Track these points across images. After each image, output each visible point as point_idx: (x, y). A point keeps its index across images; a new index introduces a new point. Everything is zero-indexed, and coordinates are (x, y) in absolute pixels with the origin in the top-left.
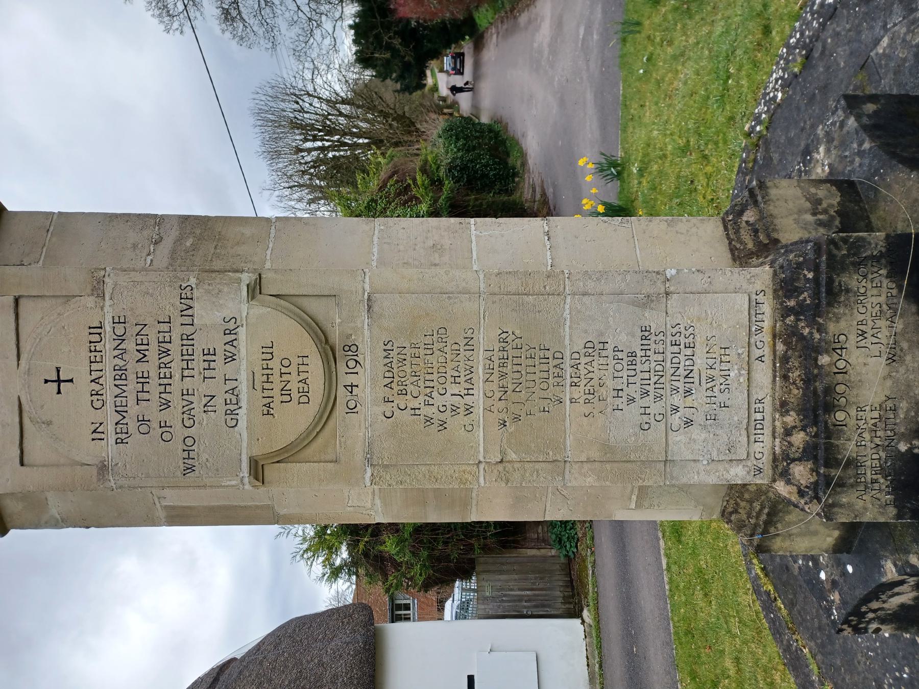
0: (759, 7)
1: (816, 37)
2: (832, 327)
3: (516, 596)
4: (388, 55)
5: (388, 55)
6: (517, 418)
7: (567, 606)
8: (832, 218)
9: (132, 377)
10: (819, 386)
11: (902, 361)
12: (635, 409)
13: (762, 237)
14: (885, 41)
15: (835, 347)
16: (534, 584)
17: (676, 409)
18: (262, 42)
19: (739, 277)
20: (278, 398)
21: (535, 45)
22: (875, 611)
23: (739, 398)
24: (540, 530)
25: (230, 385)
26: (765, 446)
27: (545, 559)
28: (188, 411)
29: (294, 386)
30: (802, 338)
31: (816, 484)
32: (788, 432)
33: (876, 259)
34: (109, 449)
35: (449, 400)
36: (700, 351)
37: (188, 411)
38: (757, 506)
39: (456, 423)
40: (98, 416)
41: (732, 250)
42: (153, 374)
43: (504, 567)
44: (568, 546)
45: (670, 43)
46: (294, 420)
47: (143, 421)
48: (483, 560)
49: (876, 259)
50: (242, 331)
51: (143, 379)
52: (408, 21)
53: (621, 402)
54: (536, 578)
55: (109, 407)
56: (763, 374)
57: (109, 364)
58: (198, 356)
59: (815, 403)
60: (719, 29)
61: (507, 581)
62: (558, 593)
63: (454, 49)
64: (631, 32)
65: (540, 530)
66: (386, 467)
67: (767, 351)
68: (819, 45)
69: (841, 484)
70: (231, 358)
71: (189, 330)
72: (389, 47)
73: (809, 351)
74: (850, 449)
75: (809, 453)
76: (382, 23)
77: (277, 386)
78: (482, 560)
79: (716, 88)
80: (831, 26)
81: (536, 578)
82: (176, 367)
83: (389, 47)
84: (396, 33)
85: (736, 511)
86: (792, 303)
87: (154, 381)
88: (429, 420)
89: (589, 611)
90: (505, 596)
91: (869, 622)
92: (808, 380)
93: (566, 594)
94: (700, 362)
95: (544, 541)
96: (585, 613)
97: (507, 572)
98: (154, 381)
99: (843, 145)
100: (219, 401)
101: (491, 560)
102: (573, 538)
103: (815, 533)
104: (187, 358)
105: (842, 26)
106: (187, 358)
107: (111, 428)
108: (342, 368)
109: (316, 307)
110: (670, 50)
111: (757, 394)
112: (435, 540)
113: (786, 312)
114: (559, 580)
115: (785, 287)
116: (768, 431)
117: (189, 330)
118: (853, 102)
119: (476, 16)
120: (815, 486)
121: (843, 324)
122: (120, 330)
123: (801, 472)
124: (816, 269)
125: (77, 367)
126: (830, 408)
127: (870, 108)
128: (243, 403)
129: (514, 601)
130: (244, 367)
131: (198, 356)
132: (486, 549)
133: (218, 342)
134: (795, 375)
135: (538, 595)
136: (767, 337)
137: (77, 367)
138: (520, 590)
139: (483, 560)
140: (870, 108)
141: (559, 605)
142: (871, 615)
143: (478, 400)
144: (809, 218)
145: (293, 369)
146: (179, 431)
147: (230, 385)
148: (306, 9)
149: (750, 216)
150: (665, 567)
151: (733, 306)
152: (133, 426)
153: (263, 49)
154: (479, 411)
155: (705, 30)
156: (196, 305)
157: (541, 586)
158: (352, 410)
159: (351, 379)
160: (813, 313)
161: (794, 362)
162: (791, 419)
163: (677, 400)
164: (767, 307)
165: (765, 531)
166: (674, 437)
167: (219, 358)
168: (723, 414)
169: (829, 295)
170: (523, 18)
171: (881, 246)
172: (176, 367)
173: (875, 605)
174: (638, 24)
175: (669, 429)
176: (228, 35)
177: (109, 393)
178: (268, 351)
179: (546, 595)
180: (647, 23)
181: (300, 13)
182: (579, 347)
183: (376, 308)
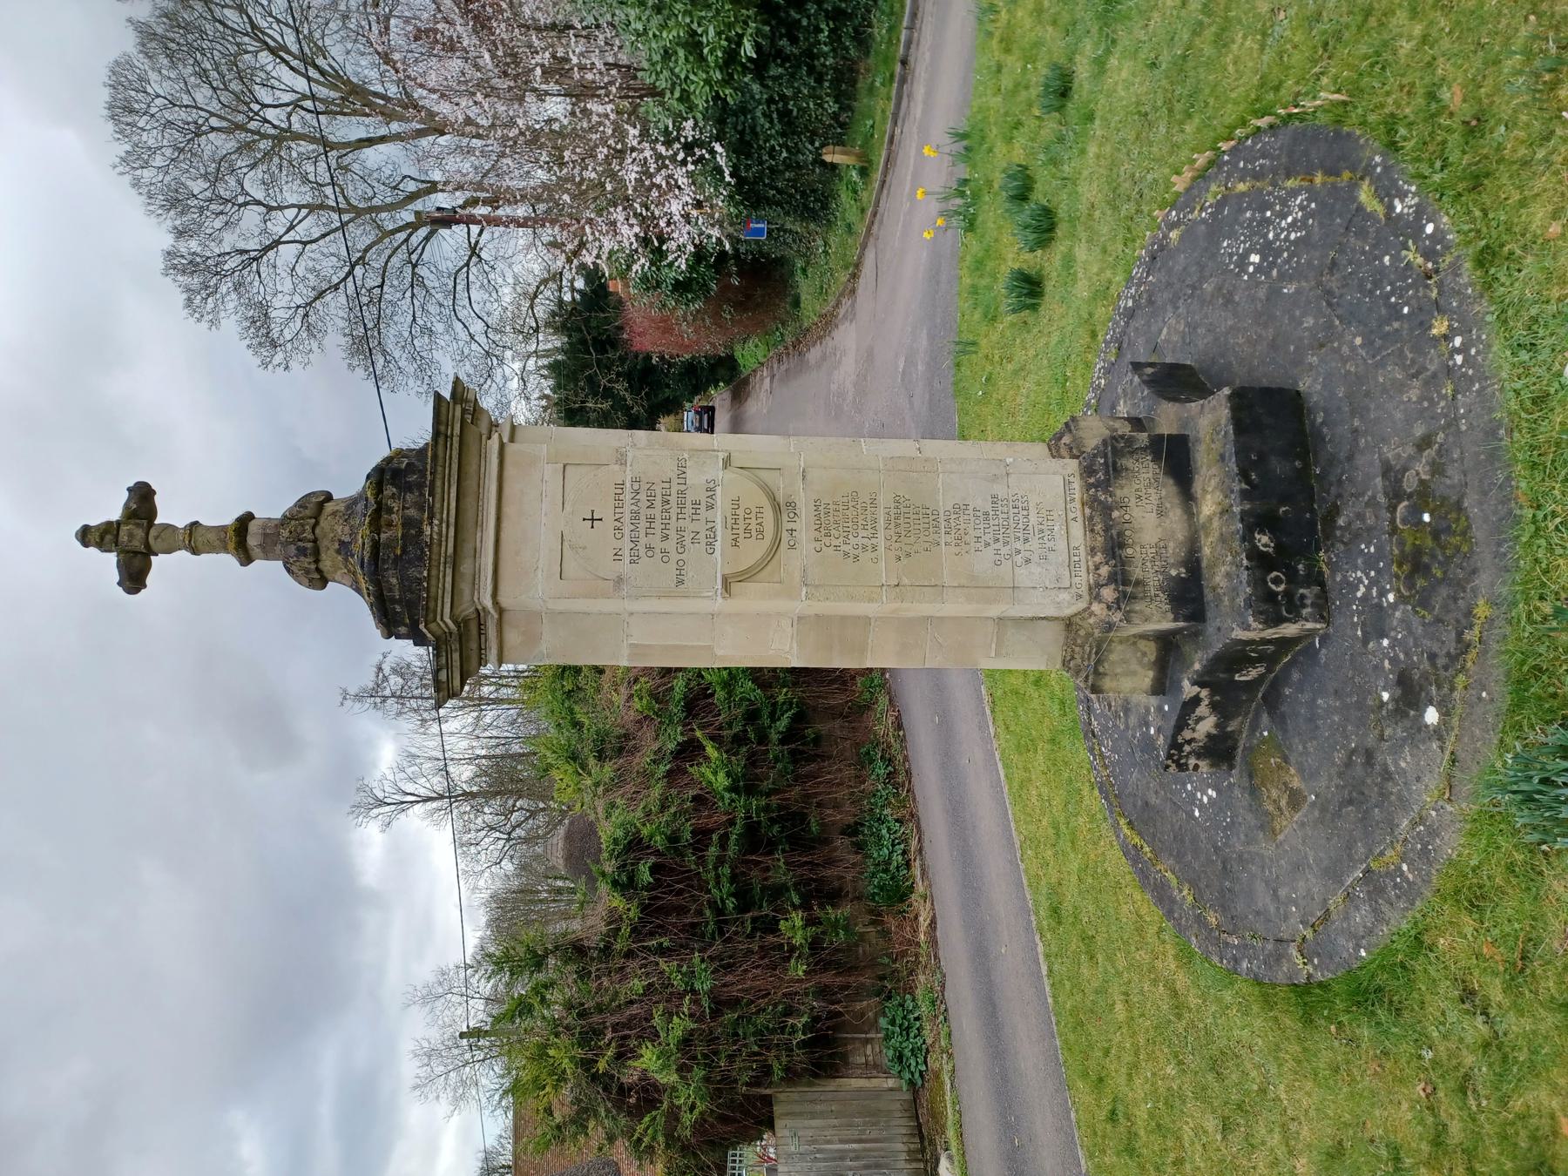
0: (1086, 316)
1: (1124, 333)
2: (1118, 493)
4: (606, 406)
5: (606, 406)
6: (909, 555)
7: (914, 1165)
9: (643, 518)
10: (1114, 532)
11: (1166, 515)
12: (990, 551)
14: (1165, 331)
15: (1121, 505)
17: (1019, 552)
18: (411, 382)
19: (1056, 464)
20: (742, 535)
21: (834, 387)
23: (1061, 545)
24: (869, 1052)
26: (1083, 580)
27: (877, 1094)
28: (680, 543)
29: (753, 527)
30: (1100, 502)
31: (1118, 599)
32: (1097, 568)
33: (1144, 449)
34: (625, 567)
35: (860, 541)
36: (1033, 512)
37: (680, 543)
38: (1087, 649)
39: (865, 557)
40: (618, 544)
42: (658, 516)
43: (819, 1108)
44: (913, 1062)
45: (1010, 360)
46: (753, 551)
47: (650, 548)
48: (786, 1100)
49: (1144, 449)
50: (719, 489)
51: (651, 520)
52: (648, 358)
53: (980, 546)
54: (865, 1124)
55: (627, 538)
56: (1077, 530)
57: (628, 508)
59: (1114, 546)
60: (1055, 338)
61: (823, 1128)
63: (698, 401)
64: (964, 352)
65: (869, 1052)
66: (817, 586)
67: (1079, 514)
68: (1126, 339)
69: (1133, 597)
70: (710, 507)
71: (682, 487)
72: (608, 393)
73: (1106, 510)
74: (1137, 573)
75: (1112, 579)
76: (599, 362)
77: (742, 526)
78: (782, 1097)
79: (1055, 393)
80: (1133, 324)
81: (865, 1124)
82: (674, 511)
83: (608, 393)
84: (618, 374)
85: (1073, 658)
86: (1092, 480)
87: (658, 521)
88: (846, 554)
89: (950, 1158)
90: (819, 1151)
91: (1187, 757)
92: (1107, 529)
94: (1033, 520)
95: (876, 1066)
97: (822, 1115)
98: (658, 521)
99: (1134, 396)
100: (702, 536)
101: (795, 1096)
102: (920, 1049)
103: (1134, 673)
105: (1138, 323)
107: (627, 552)
108: (785, 518)
109: (764, 475)
110: (1009, 367)
112: (716, 1053)
113: (1089, 486)
114: (901, 1126)
115: (1088, 471)
116: (1084, 569)
117: (682, 487)
118: (1137, 367)
119: (738, 355)
120: (1117, 601)
121: (1126, 491)
122: (636, 486)
123: (1108, 593)
124: (1105, 456)
125: (605, 511)
126: (1122, 546)
127: (1149, 370)
129: (834, 1159)
132: (792, 1076)
133: (702, 496)
134: (1098, 528)
136: (1079, 506)
137: (605, 511)
138: (842, 1141)
139: (786, 1100)
140: (1149, 370)
141: (902, 1165)
142: (1187, 748)
143: (881, 541)
145: (753, 516)
146: (674, 556)
148: (482, 339)
149: (1066, 439)
150: (1045, 972)
151: (1052, 484)
152: (642, 551)
153: (412, 393)
154: (881, 549)
155: (1043, 341)
156: (688, 471)
157: (874, 1135)
158: (792, 547)
160: (1105, 485)
161: (1097, 519)
162: (1099, 558)
163: (1019, 545)
164: (1077, 485)
165: (1096, 673)
166: (1017, 570)
168: (1051, 556)
169: (1115, 471)
170: (814, 354)
172: (674, 511)
173: (1187, 734)
174: (974, 344)
175: (1014, 565)
176: (360, 372)
177: (627, 530)
178: (736, 503)
179: (882, 1149)
180: (983, 342)
181: (474, 346)
182: (949, 507)
183: (809, 477)
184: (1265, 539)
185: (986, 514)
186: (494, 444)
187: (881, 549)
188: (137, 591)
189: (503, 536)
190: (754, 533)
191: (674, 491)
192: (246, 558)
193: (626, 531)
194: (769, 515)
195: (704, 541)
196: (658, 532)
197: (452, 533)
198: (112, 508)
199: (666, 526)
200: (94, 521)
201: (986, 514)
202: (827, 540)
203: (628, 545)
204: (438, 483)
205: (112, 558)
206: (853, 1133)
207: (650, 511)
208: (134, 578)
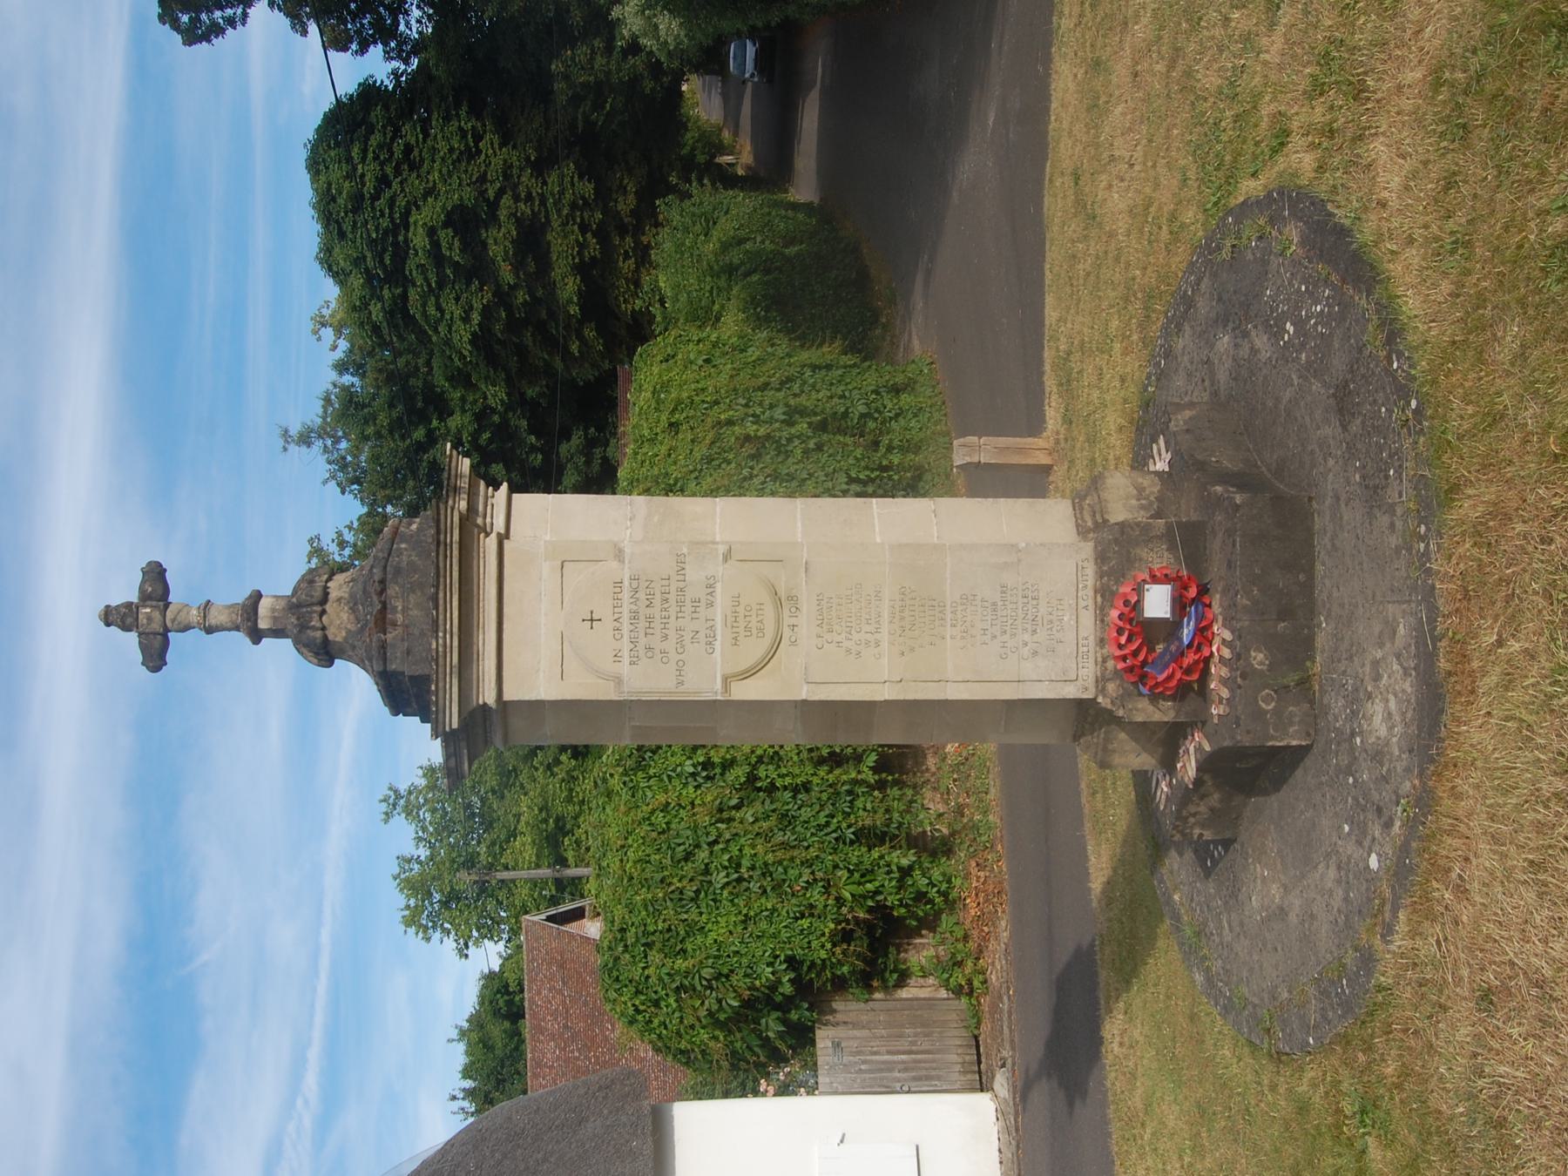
3: (883, 1062)
6: (912, 649)
7: (969, 1076)
8: (1151, 504)
9: (642, 618)
13: (1098, 517)
16: (913, 1043)
20: (743, 633)
22: (1194, 815)
23: (1070, 636)
25: (710, 623)
26: (1089, 672)
28: (680, 642)
29: (754, 624)
32: (1104, 661)
33: (1160, 538)
37: (680, 642)
41: (1077, 526)
42: (657, 616)
46: (754, 650)
49: (1160, 538)
50: (719, 585)
54: (916, 1035)
55: (626, 639)
57: (625, 610)
58: (688, 603)
62: (953, 1058)
67: (1090, 602)
70: (711, 604)
71: (681, 584)
77: (742, 624)
82: (673, 610)
88: (848, 651)
93: (967, 1058)
94: (1043, 610)
96: (997, 1086)
100: (701, 635)
104: (680, 604)
106: (680, 604)
108: (786, 613)
111: (1082, 634)
116: (1092, 660)
117: (681, 584)
122: (635, 584)
125: (604, 610)
128: (719, 637)
129: (881, 1070)
130: (719, 610)
131: (688, 603)
135: (920, 1061)
136: (1091, 593)
137: (604, 610)
138: (889, 1053)
141: (956, 1076)
142: (1192, 820)
144: (1134, 502)
145: (753, 613)
147: (710, 623)
152: (642, 653)
154: (885, 645)
158: (794, 643)
159: (793, 621)
163: (1027, 637)
164: (1090, 570)
167: (703, 604)
171: (1163, 530)
172: (673, 610)
177: (626, 628)
178: (737, 600)
179: (934, 1061)
184: (1261, 656)
185: (994, 604)
187: (885, 645)
190: (754, 631)
191: (673, 589)
192: (256, 636)
193: (625, 631)
194: (769, 612)
196: (658, 631)
197: (456, 643)
198: (126, 591)
199: (665, 626)
200: (116, 601)
201: (994, 604)
202: (828, 637)
203: (626, 645)
204: (441, 595)
205: (133, 637)
207: (649, 611)
208: (155, 657)
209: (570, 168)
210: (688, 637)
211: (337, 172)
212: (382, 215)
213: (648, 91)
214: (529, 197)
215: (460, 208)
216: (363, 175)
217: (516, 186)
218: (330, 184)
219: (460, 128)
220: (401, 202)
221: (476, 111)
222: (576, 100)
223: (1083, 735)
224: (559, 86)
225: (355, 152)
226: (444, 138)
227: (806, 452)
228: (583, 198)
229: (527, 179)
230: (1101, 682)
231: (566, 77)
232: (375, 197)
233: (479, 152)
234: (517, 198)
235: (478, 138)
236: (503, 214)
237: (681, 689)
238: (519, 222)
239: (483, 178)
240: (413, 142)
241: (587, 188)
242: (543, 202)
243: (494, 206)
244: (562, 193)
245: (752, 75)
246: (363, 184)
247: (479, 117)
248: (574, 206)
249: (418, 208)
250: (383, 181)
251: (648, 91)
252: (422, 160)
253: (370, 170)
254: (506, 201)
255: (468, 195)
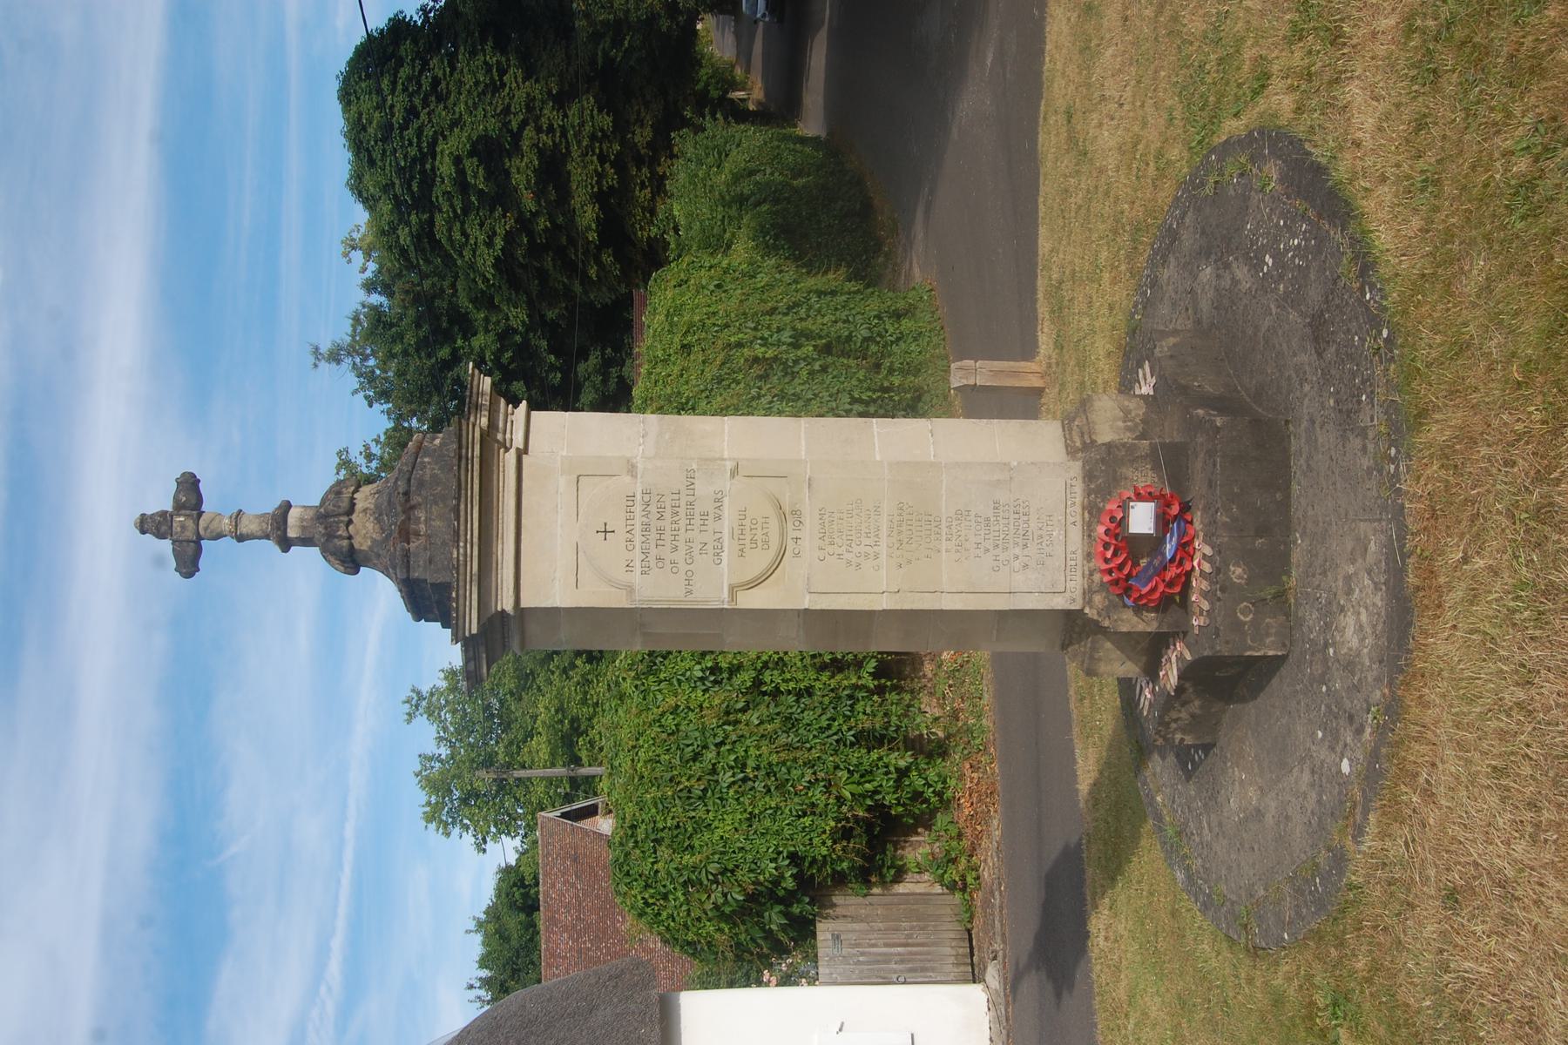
6: (909, 562)
20: (748, 546)
23: (1060, 550)
28: (689, 553)
29: (759, 537)
31: (1107, 608)
32: (1091, 574)
33: (1144, 457)
35: (862, 549)
37: (689, 553)
42: (668, 528)
46: (759, 561)
47: (660, 559)
49: (1144, 457)
50: (726, 500)
51: (661, 531)
70: (719, 518)
71: (691, 499)
77: (748, 538)
82: (683, 523)
88: (849, 563)
94: (1033, 525)
98: (668, 532)
100: (709, 547)
104: (690, 517)
106: (690, 517)
108: (790, 524)
116: (1079, 573)
122: (647, 498)
125: (617, 524)
129: (878, 962)
133: (709, 507)
136: (1079, 510)
138: (886, 945)
142: (1174, 725)
146: (683, 567)
152: (653, 563)
154: (883, 557)
157: (919, 940)
158: (797, 555)
163: (1017, 551)
164: (1079, 488)
165: (1091, 658)
167: (711, 516)
172: (683, 523)
178: (743, 514)
179: (928, 953)
184: (1239, 571)
185: (988, 519)
186: (510, 458)
187: (883, 557)
188: (189, 575)
189: (524, 521)
191: (683, 504)
195: (711, 551)
196: (668, 544)
198: (161, 499)
201: (988, 519)
202: (830, 549)
204: (462, 507)
206: (900, 937)
207: (660, 523)
208: (188, 563)
209: (589, 101)
210: (696, 551)
211: (367, 103)
212: (411, 144)
213: (664, 29)
214: (551, 129)
215: (484, 139)
216: (392, 106)
217: (538, 118)
218: (360, 114)
219: (485, 63)
220: (428, 132)
221: (501, 47)
222: (596, 37)
223: (1071, 643)
224: (580, 23)
225: (385, 83)
226: (471, 71)
227: (811, 373)
228: (602, 130)
229: (549, 113)
230: (1088, 594)
231: (587, 15)
232: (403, 128)
233: (503, 85)
234: (539, 130)
235: (502, 72)
236: (525, 145)
237: (690, 597)
238: (541, 153)
239: (507, 110)
240: (440, 74)
241: (606, 121)
242: (564, 134)
243: (517, 137)
244: (582, 124)
245: (764, 15)
246: (393, 115)
247: (503, 52)
248: (593, 137)
249: (445, 138)
250: (412, 112)
251: (664, 29)
252: (449, 93)
253: (399, 102)
254: (529, 132)
255: (493, 126)
